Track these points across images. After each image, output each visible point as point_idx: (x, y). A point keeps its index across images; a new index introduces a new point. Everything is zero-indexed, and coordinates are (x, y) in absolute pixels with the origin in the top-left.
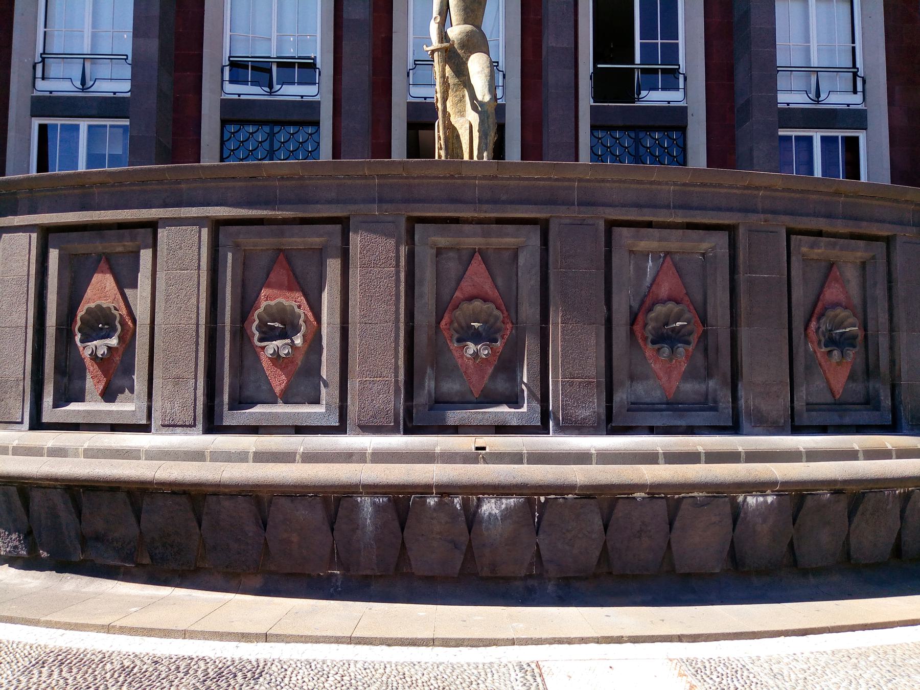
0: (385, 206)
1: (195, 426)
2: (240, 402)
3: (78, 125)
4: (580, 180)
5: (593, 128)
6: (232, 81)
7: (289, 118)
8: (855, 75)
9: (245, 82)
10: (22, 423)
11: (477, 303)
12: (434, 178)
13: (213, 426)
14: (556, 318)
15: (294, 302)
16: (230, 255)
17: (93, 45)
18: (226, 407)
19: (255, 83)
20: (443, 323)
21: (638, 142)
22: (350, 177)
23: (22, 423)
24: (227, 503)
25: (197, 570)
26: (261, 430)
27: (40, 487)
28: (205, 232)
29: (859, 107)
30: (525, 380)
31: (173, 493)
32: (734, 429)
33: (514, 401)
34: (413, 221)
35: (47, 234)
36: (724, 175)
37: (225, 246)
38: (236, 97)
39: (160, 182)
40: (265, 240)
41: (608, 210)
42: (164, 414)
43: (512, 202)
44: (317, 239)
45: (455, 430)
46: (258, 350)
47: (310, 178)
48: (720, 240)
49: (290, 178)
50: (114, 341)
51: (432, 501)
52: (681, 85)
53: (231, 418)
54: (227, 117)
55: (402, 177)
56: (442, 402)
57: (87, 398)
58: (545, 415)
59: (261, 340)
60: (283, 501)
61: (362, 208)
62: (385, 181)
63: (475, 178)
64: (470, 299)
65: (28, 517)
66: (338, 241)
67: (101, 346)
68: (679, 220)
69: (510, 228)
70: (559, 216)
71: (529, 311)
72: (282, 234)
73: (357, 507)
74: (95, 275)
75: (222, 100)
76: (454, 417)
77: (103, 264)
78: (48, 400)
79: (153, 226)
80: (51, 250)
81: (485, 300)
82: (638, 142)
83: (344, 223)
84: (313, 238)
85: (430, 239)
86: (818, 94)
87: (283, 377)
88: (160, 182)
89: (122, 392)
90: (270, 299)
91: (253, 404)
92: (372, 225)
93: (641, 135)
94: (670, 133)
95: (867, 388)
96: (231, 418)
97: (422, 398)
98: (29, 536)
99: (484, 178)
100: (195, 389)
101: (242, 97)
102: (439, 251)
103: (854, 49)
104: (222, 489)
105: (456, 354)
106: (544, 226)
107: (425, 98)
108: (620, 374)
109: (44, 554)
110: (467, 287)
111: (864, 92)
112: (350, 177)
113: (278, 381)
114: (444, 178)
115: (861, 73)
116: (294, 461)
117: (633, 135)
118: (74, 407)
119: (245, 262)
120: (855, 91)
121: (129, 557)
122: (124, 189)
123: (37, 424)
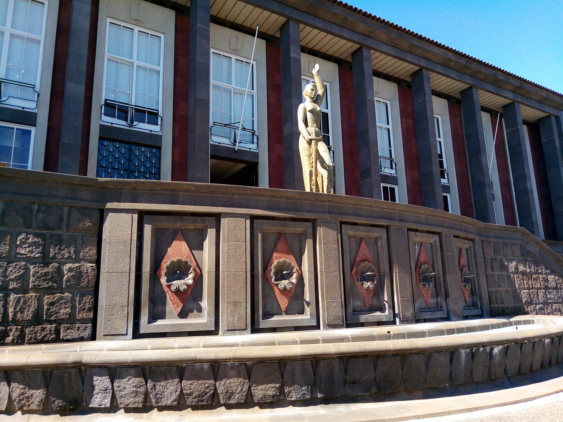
0: (332, 215)
1: (246, 329)
2: (267, 315)
3: (30, 131)
4: (399, 210)
5: (101, 138)
6: (105, 115)
7: (143, 142)
8: (253, 134)
9: (114, 116)
10: (126, 334)
11: (366, 263)
12: (350, 204)
13: (255, 330)
14: (396, 271)
15: (291, 260)
16: (260, 235)
17: (7, 74)
18: (261, 318)
19: (119, 118)
20: (353, 272)
21: (130, 150)
22: (317, 200)
23: (126, 334)
24: (416, 358)
25: (394, 393)
26: (278, 330)
27: (324, 359)
28: (248, 222)
29: (255, 151)
30: (386, 299)
31: (393, 355)
32: (448, 319)
33: (382, 310)
34: (342, 223)
35: (143, 215)
36: (354, 199)
37: (257, 230)
38: (110, 125)
39: (223, 193)
40: (276, 228)
41: (408, 224)
42: (228, 324)
43: (377, 218)
44: (300, 229)
45: (362, 325)
46: (273, 286)
47: (300, 199)
48: (436, 238)
49: (291, 198)
50: (190, 282)
51: (481, 349)
52: (159, 123)
53: (264, 324)
54: (104, 136)
55: (338, 203)
56: (357, 312)
57: (167, 316)
58: (395, 315)
59: (276, 280)
60: (436, 354)
61: (323, 216)
62: (331, 204)
63: (365, 206)
64: (363, 261)
65: (427, 366)
66: (310, 231)
67: (180, 284)
68: (364, 222)
69: (376, 229)
70: (394, 224)
71: (385, 267)
72: (285, 226)
73: (460, 354)
74: (175, 243)
75: (101, 125)
76: (363, 318)
77: (179, 235)
78: (144, 319)
79: (218, 217)
80: (146, 225)
81: (369, 262)
82: (130, 150)
83: (314, 223)
84: (299, 228)
85: (349, 231)
86: (235, 141)
87: (286, 300)
88: (223, 193)
89: (192, 312)
90: (277, 259)
91: (272, 315)
92: (327, 224)
93: (133, 147)
94: (115, 144)
95: (473, 300)
96: (264, 324)
97: (350, 310)
98: (314, 386)
99: (368, 206)
100: (246, 308)
101: (114, 125)
102: (350, 237)
103: (253, 120)
104: (412, 351)
105: (359, 287)
106: (387, 228)
107: (151, 131)
108: (416, 297)
109: (319, 395)
110: (361, 256)
111: (257, 143)
112: (317, 200)
113: (283, 302)
114: (354, 204)
115: (256, 133)
116: (297, 344)
117: (128, 146)
118: (160, 322)
119: (156, 233)
120: (392, 168)
121: (368, 390)
122: (200, 194)
123: (137, 335)
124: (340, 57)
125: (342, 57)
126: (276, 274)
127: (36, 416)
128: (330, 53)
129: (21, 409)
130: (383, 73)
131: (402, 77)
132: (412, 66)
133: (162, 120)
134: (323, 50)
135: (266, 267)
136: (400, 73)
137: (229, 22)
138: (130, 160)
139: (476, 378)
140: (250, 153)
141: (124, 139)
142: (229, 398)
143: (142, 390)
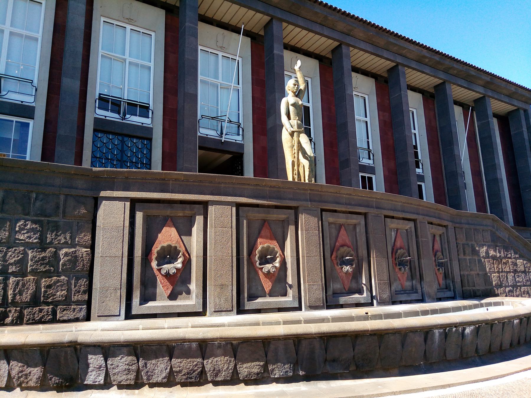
0: (313, 203)
1: (232, 310)
2: (252, 297)
3: (29, 124)
4: (376, 198)
5: (95, 130)
6: (99, 108)
7: (135, 134)
8: (239, 126)
9: (107, 110)
10: (119, 315)
11: (345, 248)
12: (331, 192)
13: (241, 311)
14: (373, 255)
15: (274, 245)
16: (245, 221)
17: (6, 69)
18: (246, 300)
19: (112, 111)
20: (333, 257)
21: (123, 142)
22: (299, 189)
23: (119, 315)
24: (392, 337)
25: (371, 371)
26: (262, 311)
27: (305, 338)
28: (234, 209)
29: (240, 142)
30: (364, 282)
31: (370, 335)
32: (422, 301)
33: (360, 292)
34: (322, 210)
35: (135, 203)
36: (334, 188)
37: (243, 217)
38: (104, 118)
39: (211, 182)
40: (260, 215)
41: (385, 211)
42: (215, 305)
43: (356, 205)
44: (283, 216)
45: (342, 306)
46: (258, 269)
47: (283, 188)
48: (411, 224)
49: (274, 187)
50: (180, 266)
51: (454, 329)
52: (150, 116)
53: (249, 305)
54: (98, 128)
55: (319, 191)
56: (337, 294)
57: (157, 298)
58: (372, 298)
59: (260, 264)
60: (411, 334)
61: (304, 203)
62: (312, 192)
63: (344, 194)
64: (342, 246)
65: (403, 346)
66: (293, 217)
67: (170, 268)
68: (344, 209)
69: (355, 216)
70: (372, 212)
71: (363, 252)
72: (269, 213)
73: (434, 334)
74: (165, 229)
75: (95, 118)
76: (343, 300)
77: (169, 222)
78: (136, 300)
79: (205, 204)
80: (137, 212)
81: (348, 247)
82: (123, 142)
83: (296, 210)
84: (282, 215)
85: (329, 218)
86: (222, 133)
87: (270, 283)
88: (211, 182)
89: (181, 294)
90: (262, 244)
91: (256, 297)
92: (308, 211)
93: (126, 139)
94: (108, 136)
95: (446, 282)
96: (249, 305)
97: (330, 293)
98: (296, 364)
99: (347, 194)
100: (232, 291)
101: (107, 118)
102: (330, 224)
103: (239, 113)
104: (389, 331)
105: (339, 271)
106: (365, 215)
107: (142, 124)
108: (392, 280)
109: (301, 373)
110: (340, 241)
111: (243, 135)
112: (299, 189)
113: (267, 285)
114: (334, 193)
115: (242, 126)
116: (280, 324)
117: (120, 138)
118: (151, 304)
119: (147, 219)
120: (369, 158)
121: (347, 368)
122: (189, 183)
123: (129, 316)
124: (321, 54)
125: (323, 54)
126: (260, 258)
127: (34, 392)
128: (311, 50)
129: (20, 385)
130: (362, 69)
131: (379, 73)
132: (389, 62)
133: (153, 113)
134: (305, 48)
135: (251, 252)
136: (378, 69)
137: (216, 20)
138: (122, 151)
139: (449, 357)
140: (235, 144)
141: (117, 131)
142: (216, 375)
143: (134, 367)
